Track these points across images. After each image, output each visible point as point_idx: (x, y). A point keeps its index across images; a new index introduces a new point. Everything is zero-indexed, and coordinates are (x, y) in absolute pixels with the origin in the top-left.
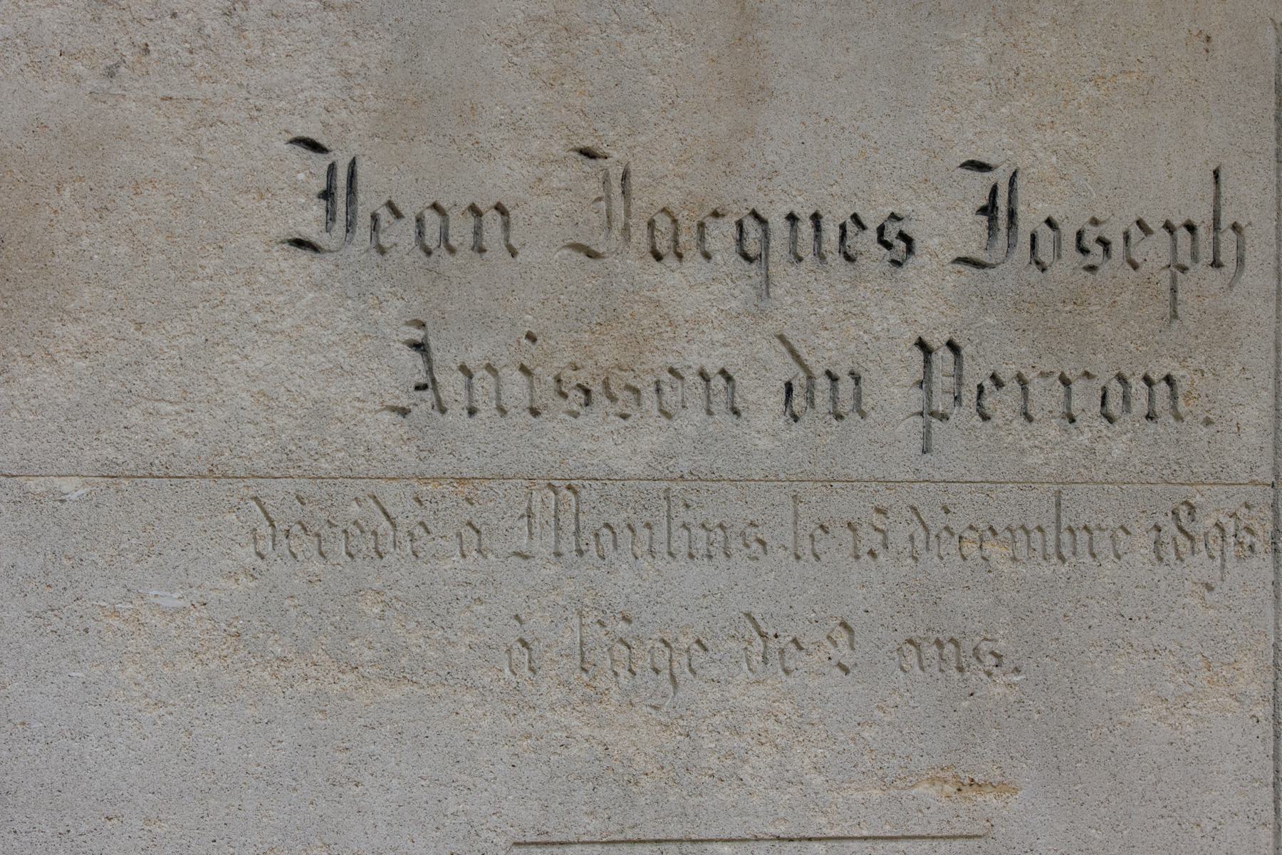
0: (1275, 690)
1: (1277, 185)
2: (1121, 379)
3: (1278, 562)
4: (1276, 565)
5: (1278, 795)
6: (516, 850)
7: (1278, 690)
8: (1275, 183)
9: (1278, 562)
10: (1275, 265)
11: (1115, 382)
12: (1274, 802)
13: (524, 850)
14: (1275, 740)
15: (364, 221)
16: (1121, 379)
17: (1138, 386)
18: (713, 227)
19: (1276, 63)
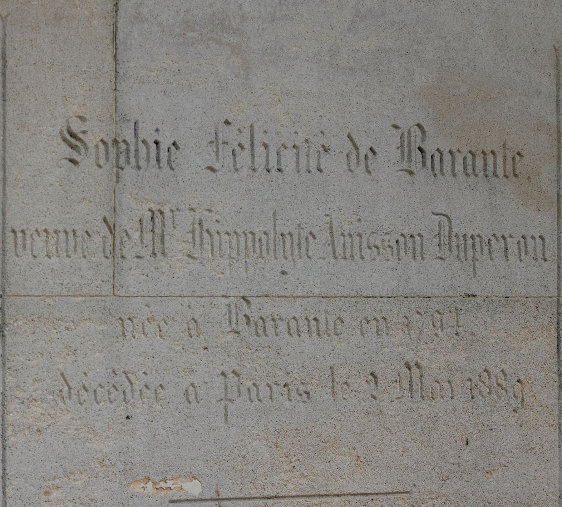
0: (3, 420)
1: (3, 115)
2: (524, 237)
3: (4, 343)
4: (3, 344)
5: (5, 484)
6: (171, 505)
7: (5, 420)
8: (2, 113)
9: (4, 343)
10: (2, 163)
11: (263, 235)
12: (3, 488)
13: (175, 504)
14: (3, 451)
15: (362, 157)
16: (524, 237)
17: (529, 240)
18: (283, 152)
19: (2, 40)
